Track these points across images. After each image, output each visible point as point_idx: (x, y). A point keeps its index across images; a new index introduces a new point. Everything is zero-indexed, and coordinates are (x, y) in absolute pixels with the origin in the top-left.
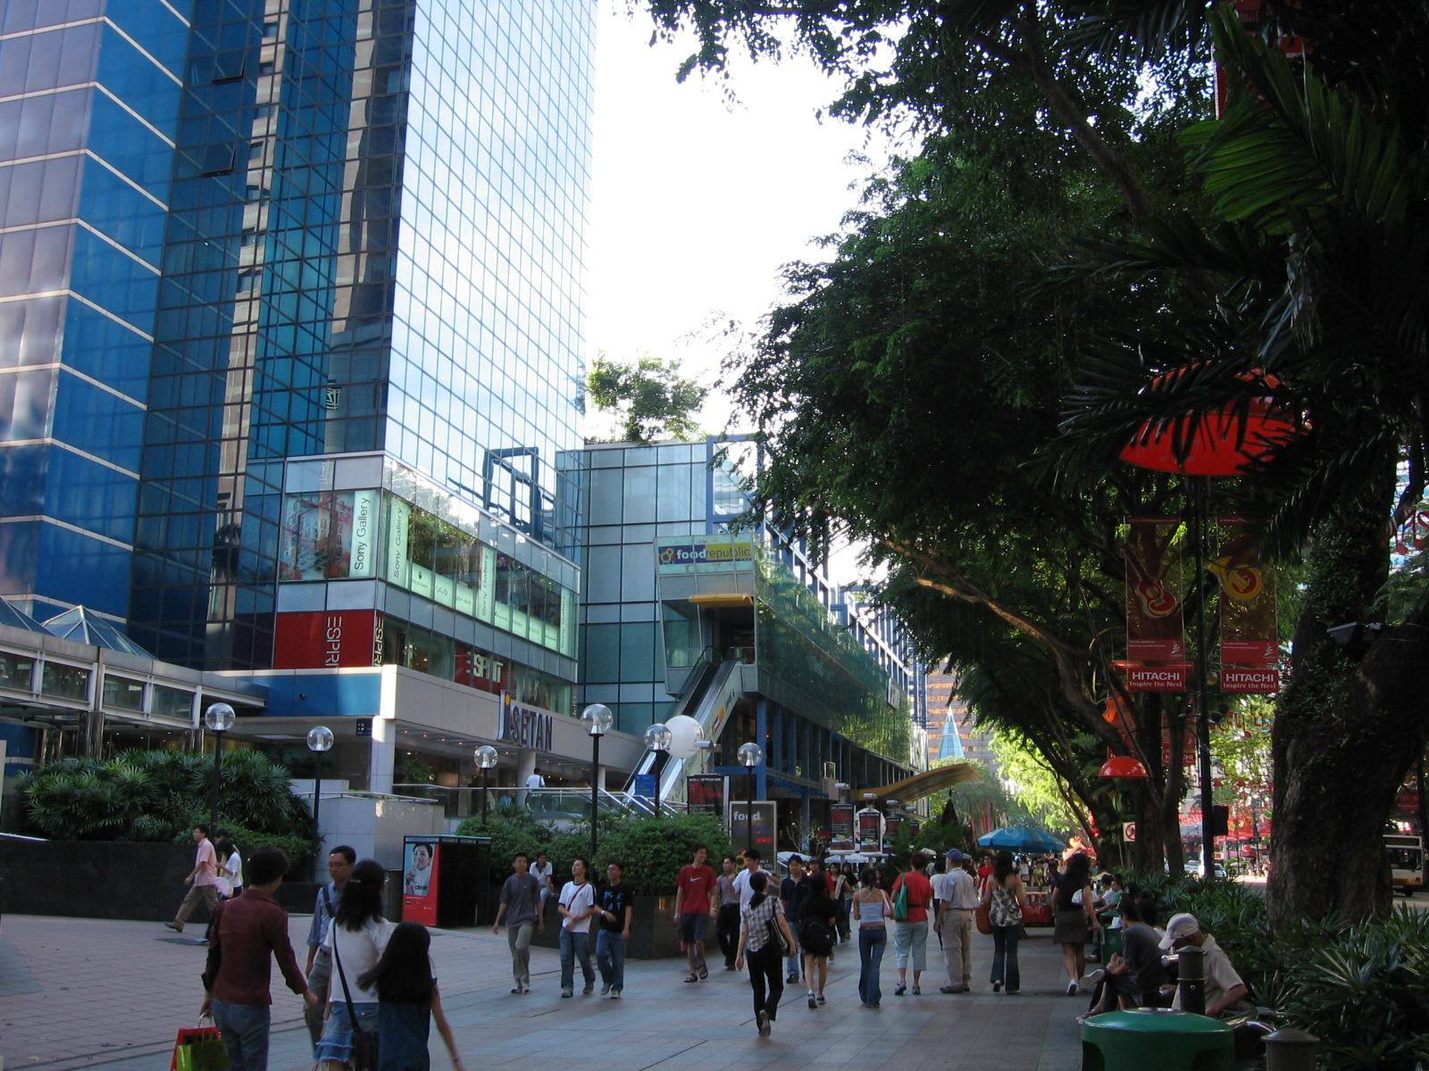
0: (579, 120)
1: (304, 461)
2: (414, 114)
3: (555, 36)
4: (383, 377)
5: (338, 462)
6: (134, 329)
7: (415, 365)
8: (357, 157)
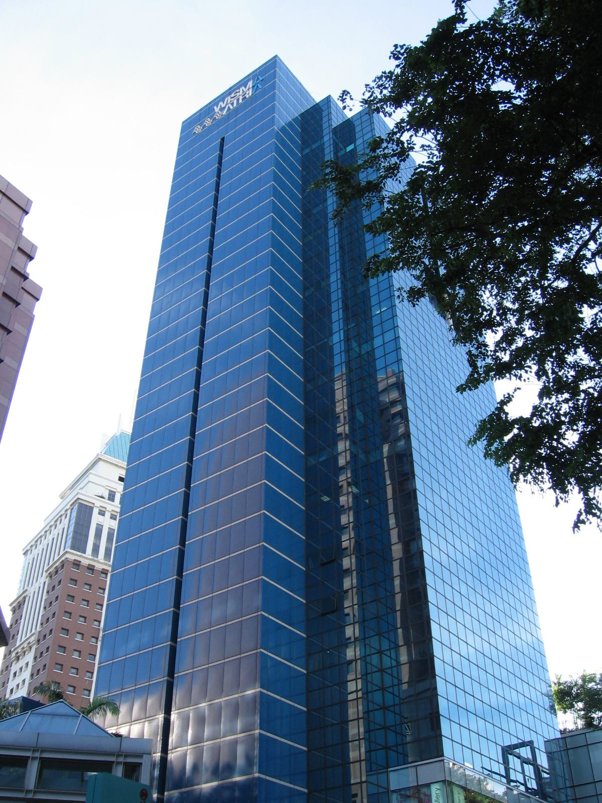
1: (398, 770)
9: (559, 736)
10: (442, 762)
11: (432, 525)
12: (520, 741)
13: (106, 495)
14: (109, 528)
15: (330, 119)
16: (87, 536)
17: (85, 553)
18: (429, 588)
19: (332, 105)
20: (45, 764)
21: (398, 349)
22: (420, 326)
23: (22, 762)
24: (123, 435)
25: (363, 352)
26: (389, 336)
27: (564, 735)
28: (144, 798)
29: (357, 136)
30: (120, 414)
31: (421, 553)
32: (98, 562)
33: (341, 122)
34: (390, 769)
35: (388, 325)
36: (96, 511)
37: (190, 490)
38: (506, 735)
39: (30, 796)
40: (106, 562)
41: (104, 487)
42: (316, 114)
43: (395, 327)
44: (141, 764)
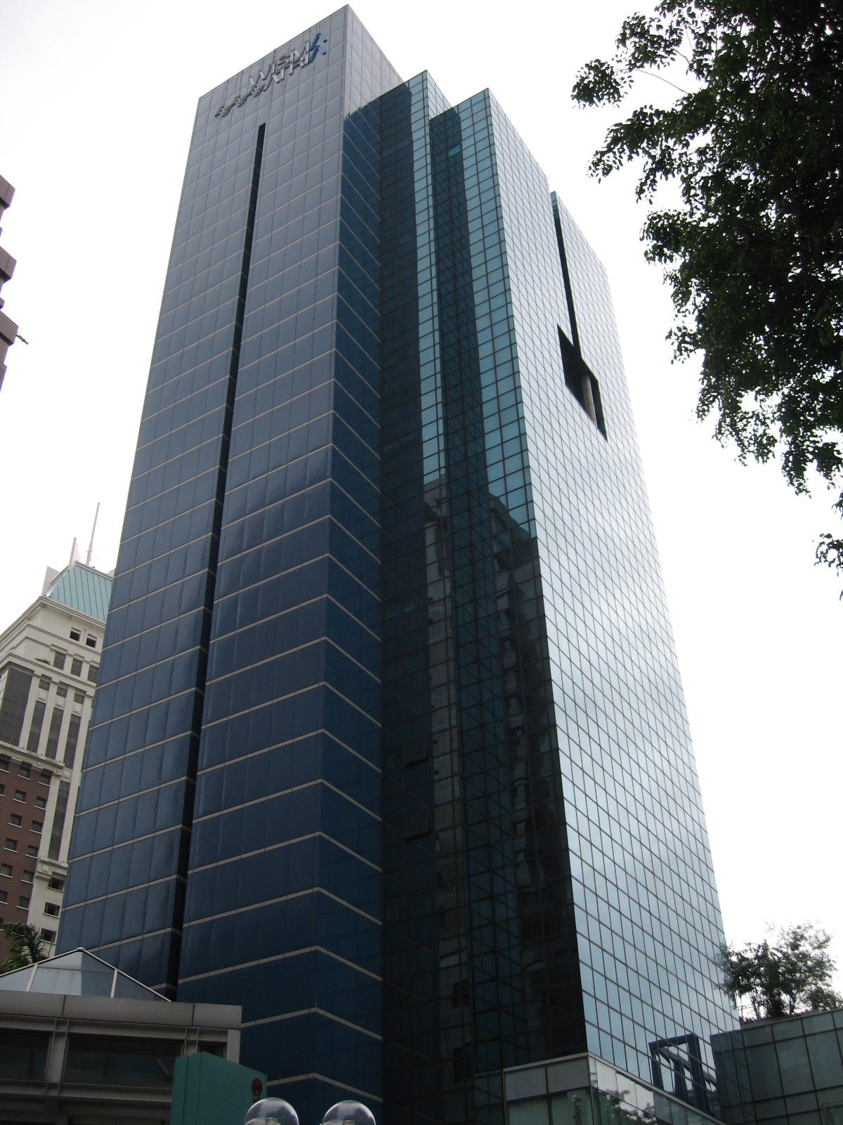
0: (712, 926)
1: (517, 1071)
2: (551, 631)
3: (663, 737)
4: (538, 594)
5: (549, 1069)
6: (337, 899)
7: (599, 973)
8: (550, 1092)
9: (738, 1027)
10: (584, 1062)
11: (571, 711)
12: (688, 1033)
13: (51, 657)
14: (55, 708)
15: (425, 107)
16: (21, 720)
17: (17, 745)
18: (566, 804)
19: (429, 86)
20: (77, 1044)
21: (523, 451)
22: (548, 417)
23: (41, 1041)
24: (80, 571)
25: (470, 454)
26: (510, 432)
27: (746, 1027)
28: (257, 1092)
29: (464, 135)
30: (75, 539)
31: (555, 750)
32: (38, 759)
33: (442, 112)
34: (506, 1070)
35: (508, 416)
36: (35, 683)
37: (208, 650)
38: (670, 1024)
39: (54, 1093)
40: (49, 759)
41: (48, 646)
42: (398, 103)
43: (520, 419)
44: (225, 1044)
